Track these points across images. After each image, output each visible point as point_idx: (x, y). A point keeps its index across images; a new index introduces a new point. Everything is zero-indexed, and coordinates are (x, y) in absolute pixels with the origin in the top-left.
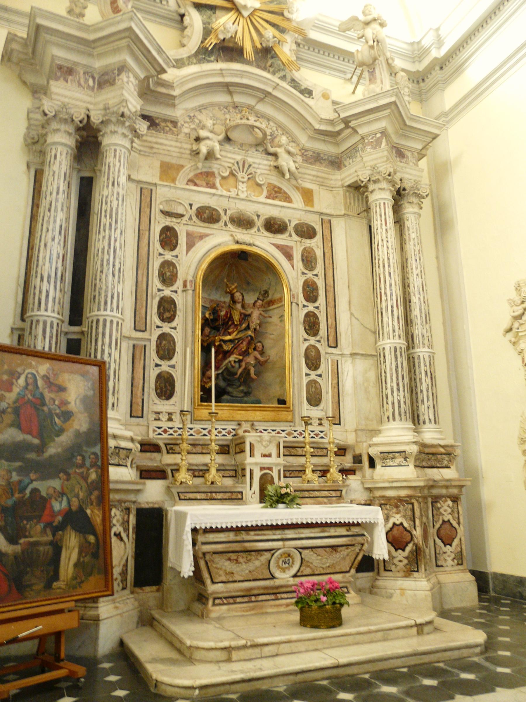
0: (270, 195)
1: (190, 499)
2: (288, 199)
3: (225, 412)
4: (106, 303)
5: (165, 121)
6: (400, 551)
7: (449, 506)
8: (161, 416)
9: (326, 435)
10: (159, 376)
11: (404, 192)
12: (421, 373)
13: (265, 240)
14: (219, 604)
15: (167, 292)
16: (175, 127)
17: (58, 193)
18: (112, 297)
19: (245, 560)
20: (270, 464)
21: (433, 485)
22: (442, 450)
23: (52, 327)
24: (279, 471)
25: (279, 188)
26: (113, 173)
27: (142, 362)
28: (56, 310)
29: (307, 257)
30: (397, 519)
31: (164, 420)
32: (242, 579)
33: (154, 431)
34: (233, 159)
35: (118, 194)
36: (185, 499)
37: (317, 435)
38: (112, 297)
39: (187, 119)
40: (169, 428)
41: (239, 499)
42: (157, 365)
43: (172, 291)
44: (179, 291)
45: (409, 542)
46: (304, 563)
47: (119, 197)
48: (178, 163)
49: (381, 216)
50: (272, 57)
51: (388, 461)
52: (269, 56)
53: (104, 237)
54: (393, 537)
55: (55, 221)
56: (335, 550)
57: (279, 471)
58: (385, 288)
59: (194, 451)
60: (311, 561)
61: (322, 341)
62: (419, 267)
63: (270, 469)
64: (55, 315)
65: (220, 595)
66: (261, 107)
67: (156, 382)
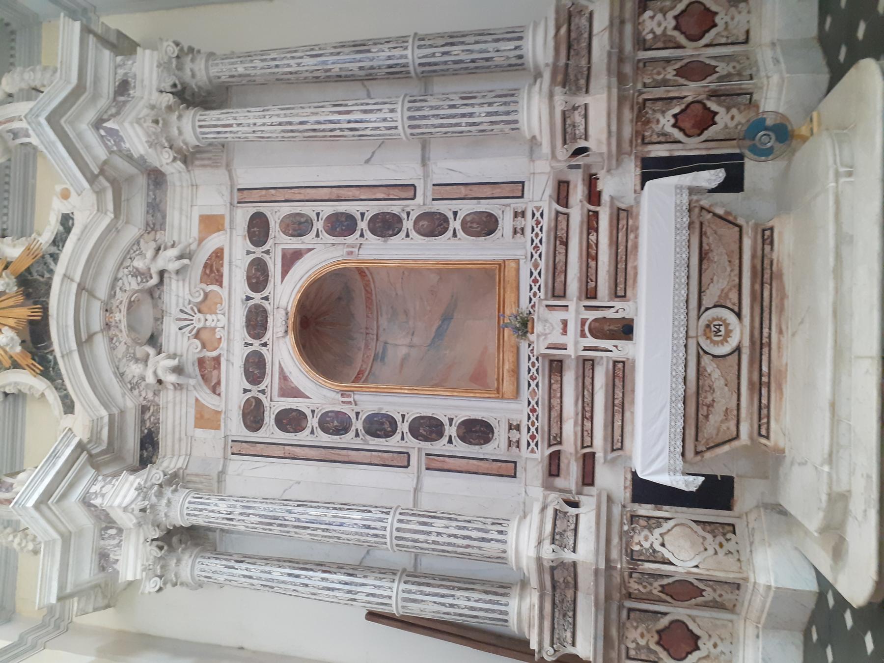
0: (217, 281)
1: (622, 436)
2: (218, 254)
3: (506, 357)
4: (376, 536)
5: (143, 422)
6: (717, 118)
7: (652, 18)
8: (514, 440)
9: (538, 208)
10: (463, 438)
11: (179, 87)
12: (446, 63)
13: (279, 287)
14: (768, 429)
15: (358, 425)
16: (149, 409)
17: (251, 577)
18: (369, 527)
19: (709, 394)
20: (576, 323)
21: (618, 57)
22: (563, 30)
23: (409, 592)
24: (587, 308)
25: (205, 266)
26: (217, 518)
27: (446, 459)
28: (389, 584)
29: (294, 230)
30: (666, 122)
31: (518, 436)
32: (735, 396)
33: (533, 451)
34: (176, 336)
35: (241, 514)
36: (622, 442)
37: (538, 223)
38: (369, 527)
39: (136, 392)
40: (528, 432)
41: (624, 367)
42: (450, 441)
43: (357, 418)
44: (357, 409)
45: (704, 105)
46: (722, 302)
47: (244, 513)
48: (194, 406)
49: (219, 133)
50: (30, 273)
51: (577, 132)
52: (29, 277)
53: (296, 533)
54: (694, 127)
55: (283, 582)
56: (706, 254)
57: (587, 308)
58: (324, 130)
59: (558, 408)
60: (719, 293)
61: (408, 209)
62: (286, 62)
63: (583, 322)
64: (395, 585)
65: (756, 426)
66: (102, 291)
67: (470, 443)
